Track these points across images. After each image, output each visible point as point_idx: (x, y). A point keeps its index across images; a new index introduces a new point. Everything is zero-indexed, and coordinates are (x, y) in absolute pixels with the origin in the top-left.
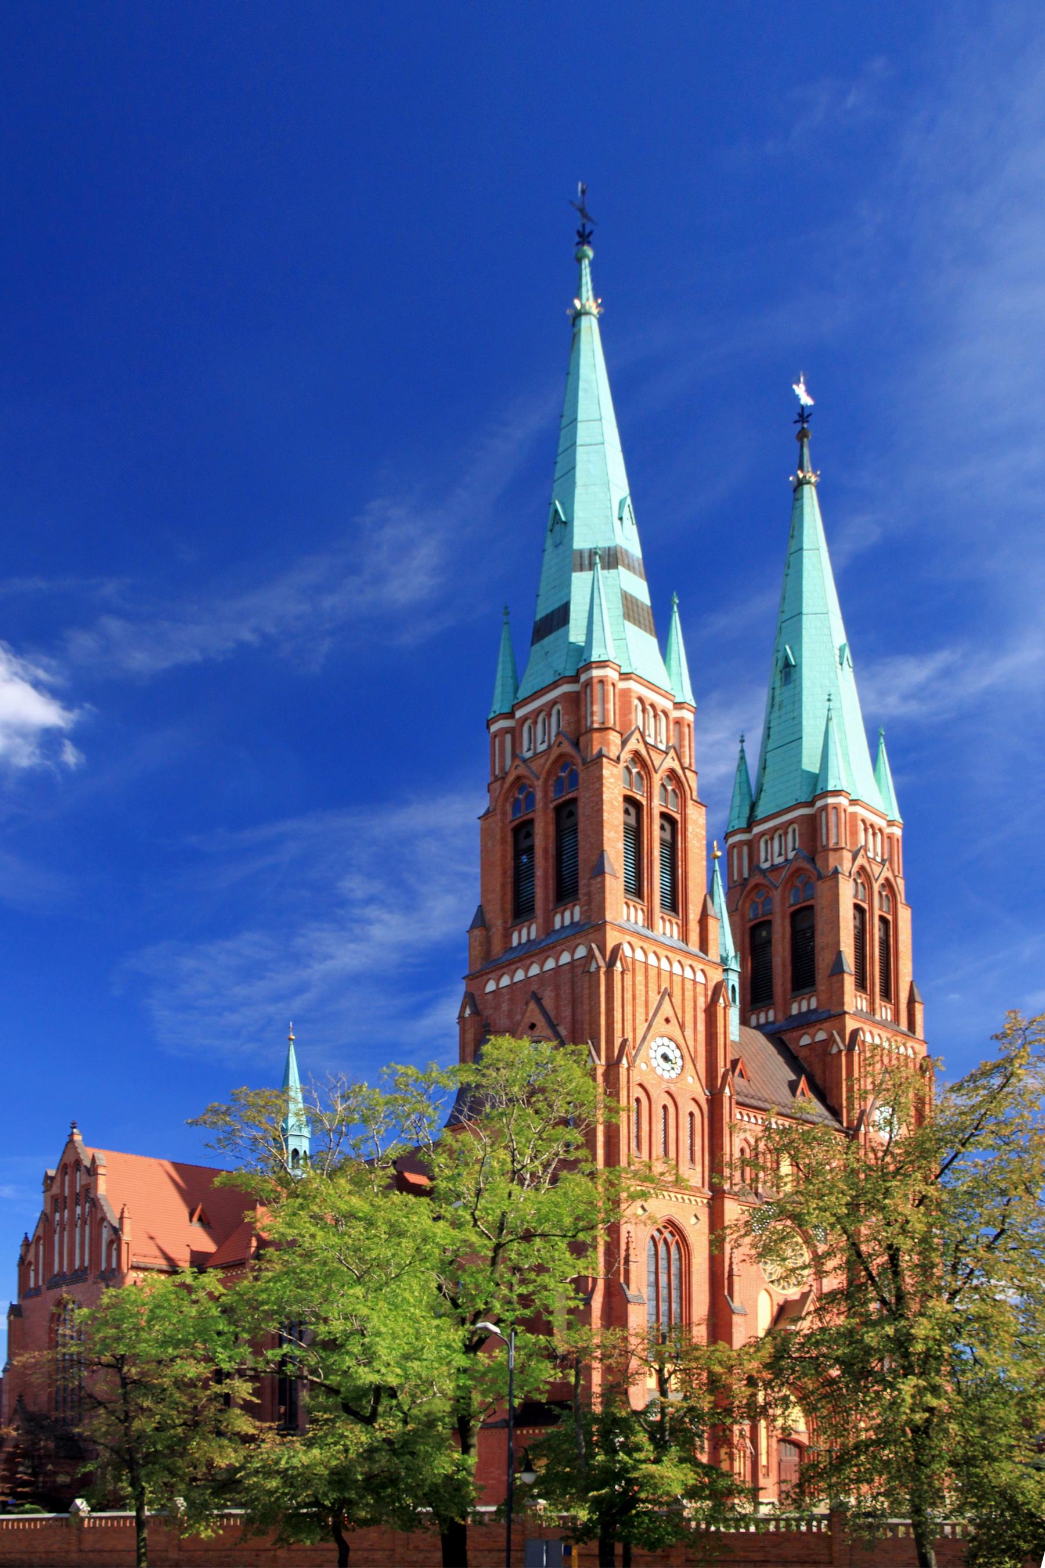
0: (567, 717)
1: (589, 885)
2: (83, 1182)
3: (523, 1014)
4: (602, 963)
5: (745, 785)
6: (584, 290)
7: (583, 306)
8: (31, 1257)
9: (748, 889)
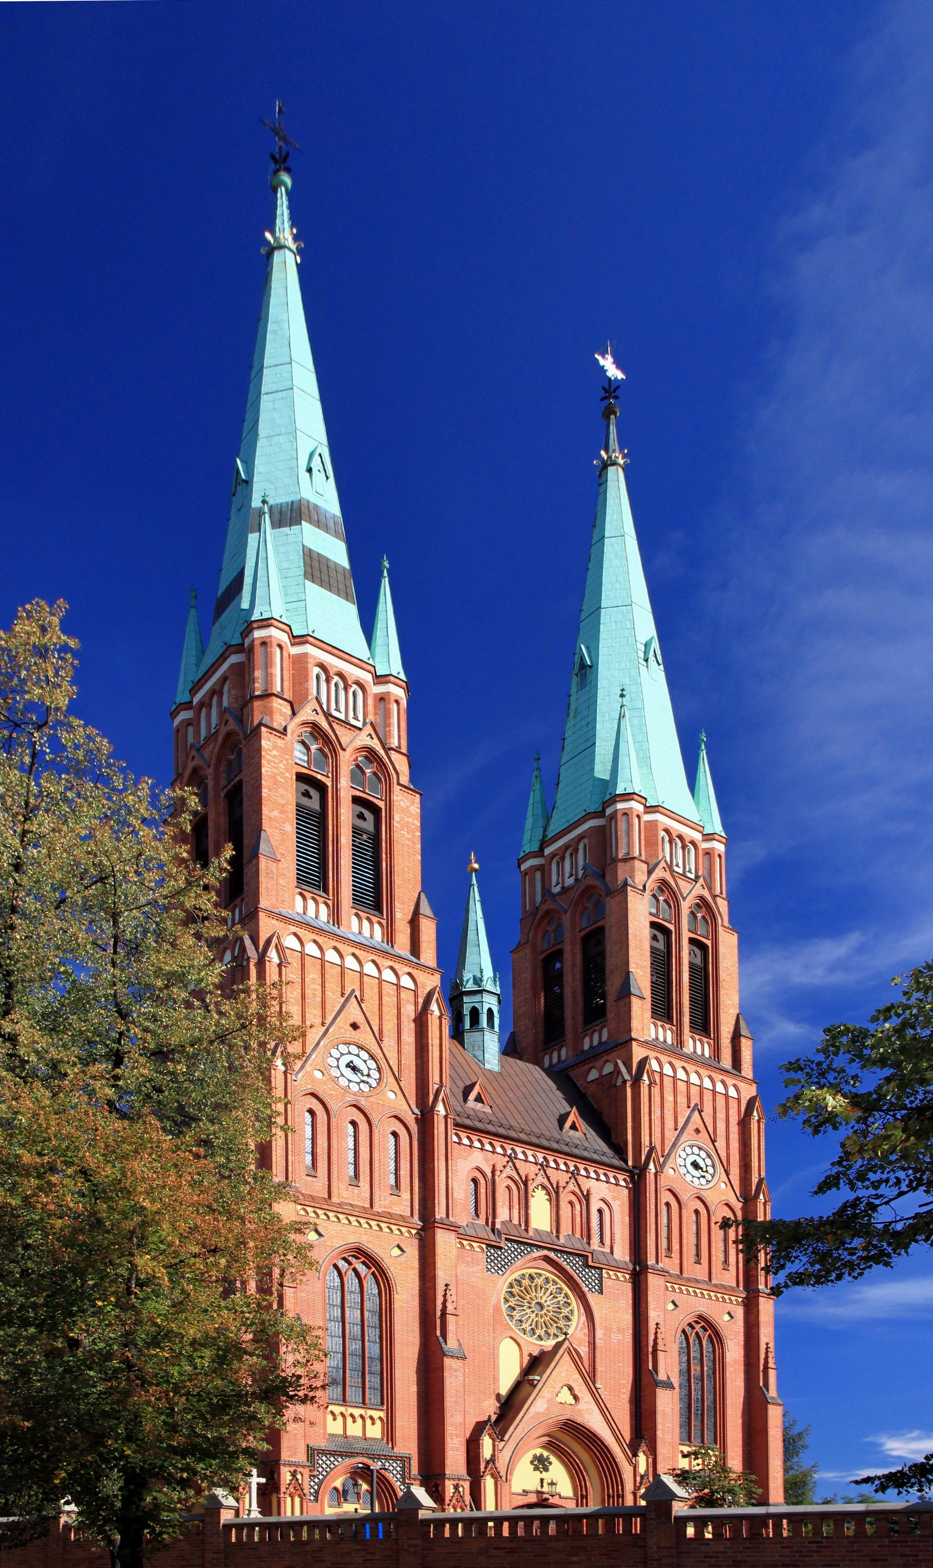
4: (627, 1077)
7: (609, 457)
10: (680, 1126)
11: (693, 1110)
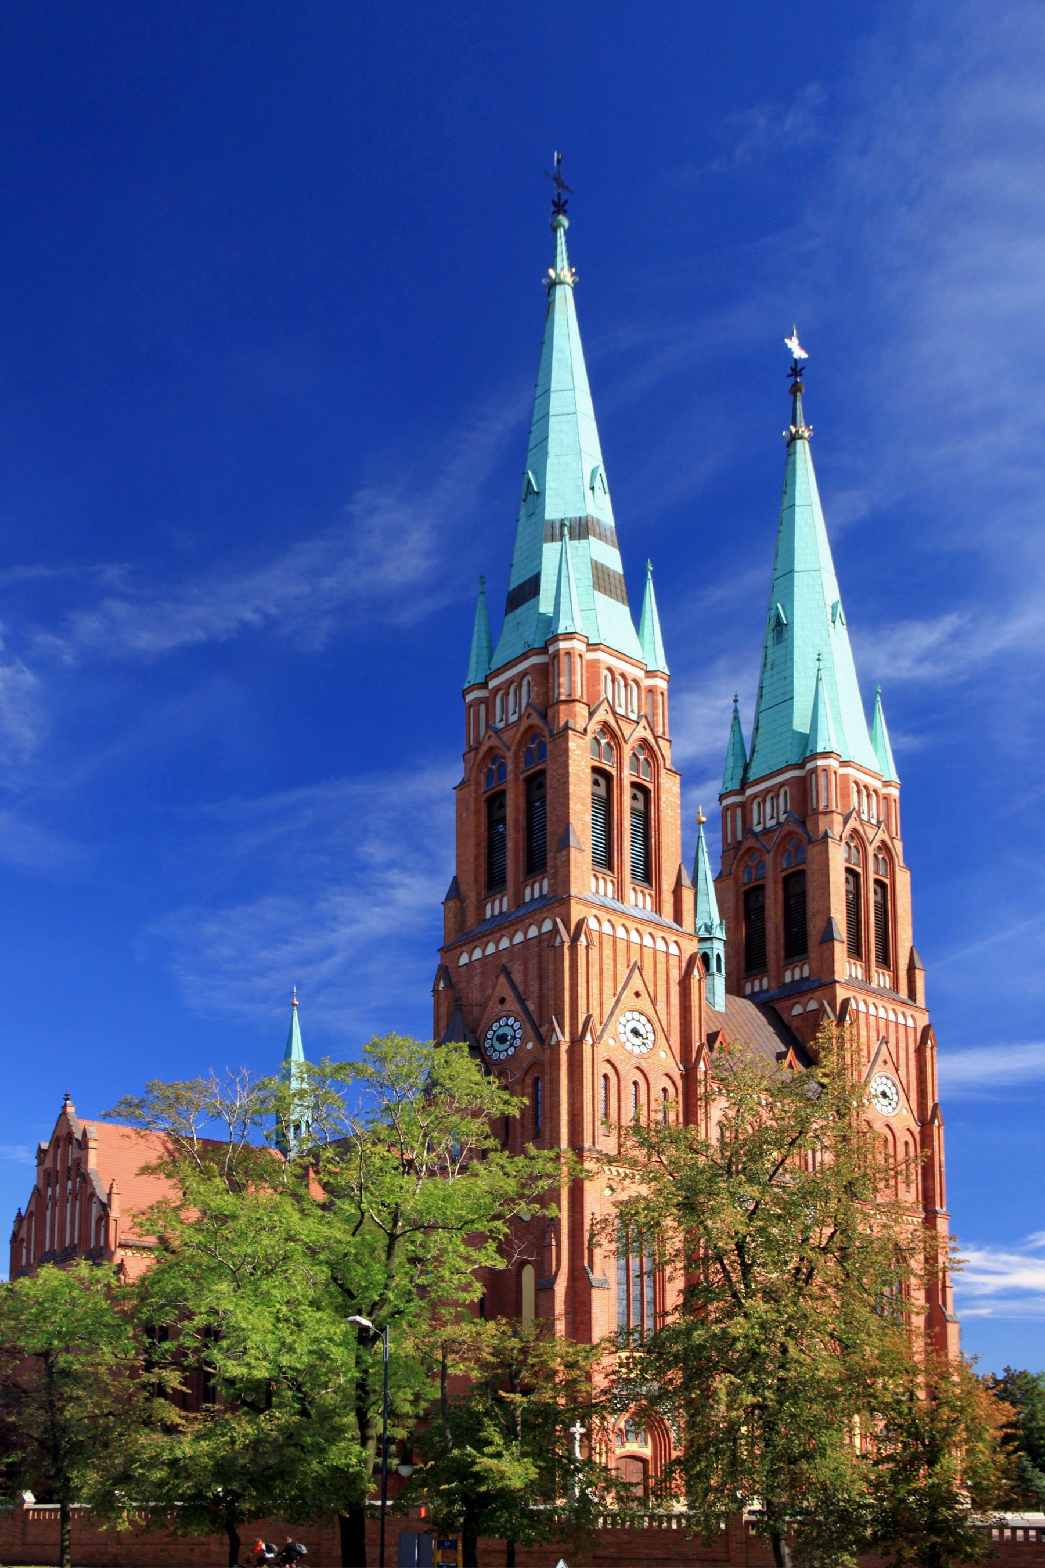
0: (536, 689)
1: (555, 859)
2: (75, 1156)
3: (494, 988)
4: (566, 938)
5: (739, 746)
6: (559, 259)
7: (557, 275)
8: (23, 1234)
9: (741, 852)
10: (872, 1057)
11: (881, 1043)
